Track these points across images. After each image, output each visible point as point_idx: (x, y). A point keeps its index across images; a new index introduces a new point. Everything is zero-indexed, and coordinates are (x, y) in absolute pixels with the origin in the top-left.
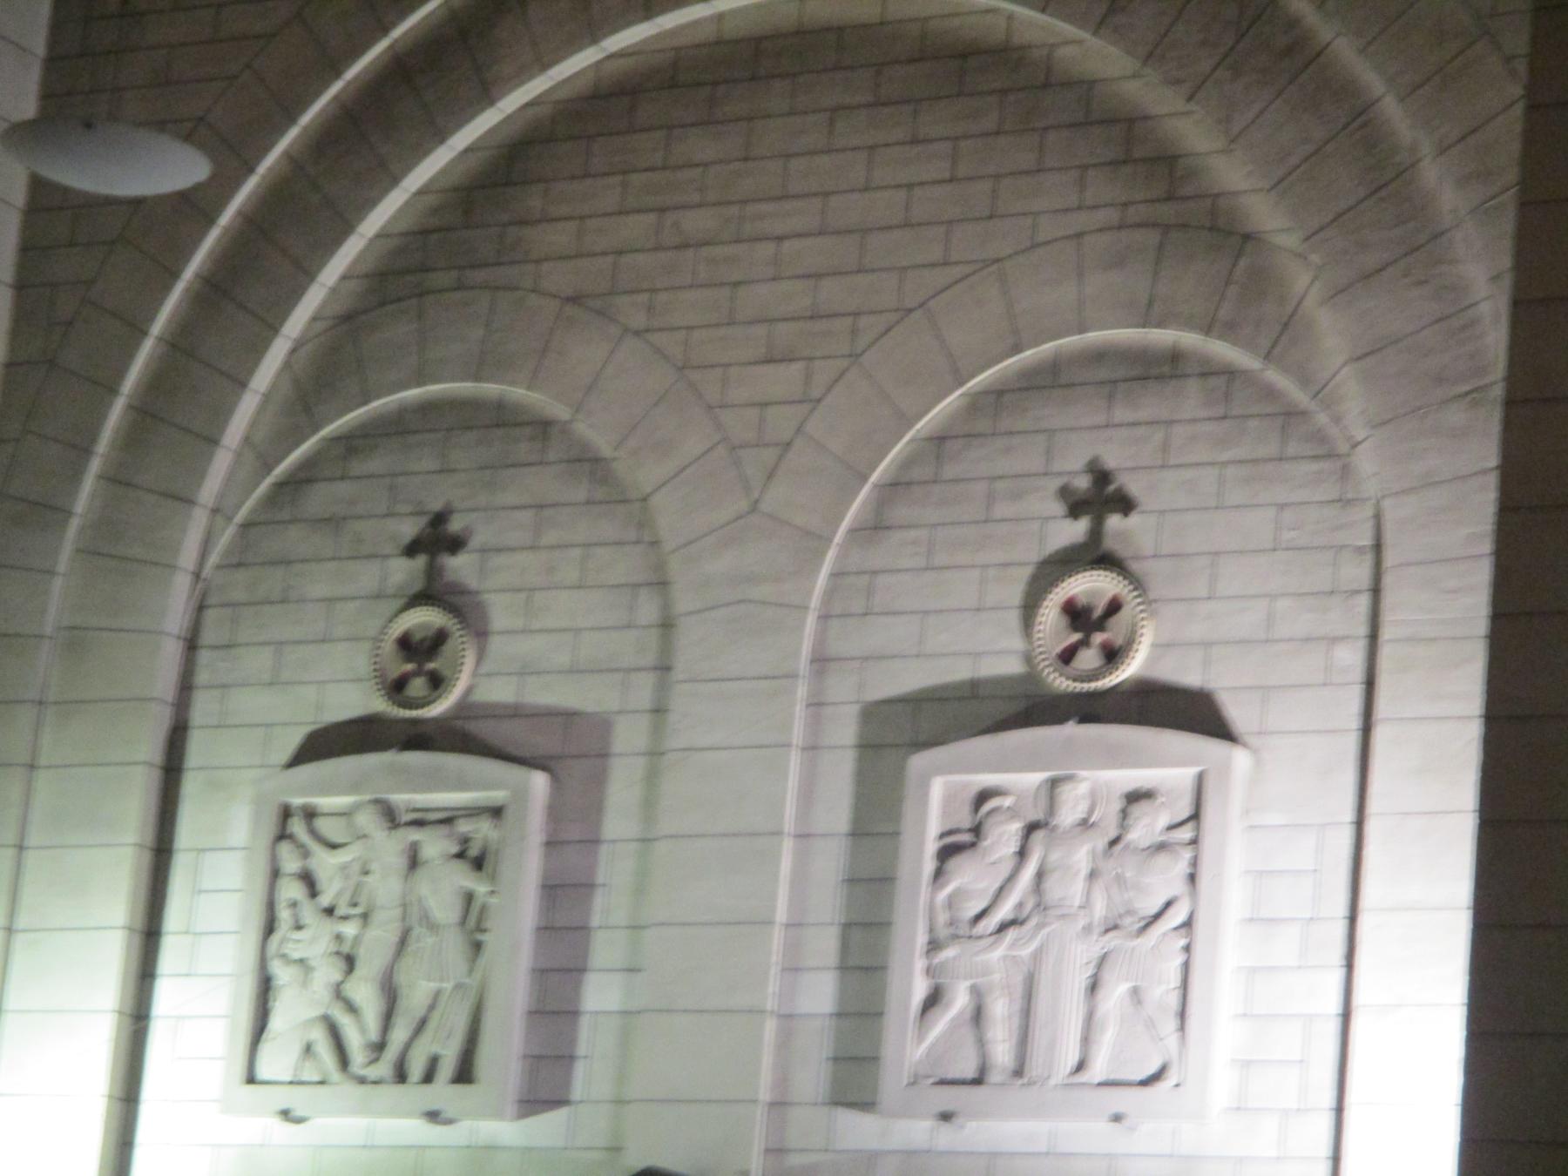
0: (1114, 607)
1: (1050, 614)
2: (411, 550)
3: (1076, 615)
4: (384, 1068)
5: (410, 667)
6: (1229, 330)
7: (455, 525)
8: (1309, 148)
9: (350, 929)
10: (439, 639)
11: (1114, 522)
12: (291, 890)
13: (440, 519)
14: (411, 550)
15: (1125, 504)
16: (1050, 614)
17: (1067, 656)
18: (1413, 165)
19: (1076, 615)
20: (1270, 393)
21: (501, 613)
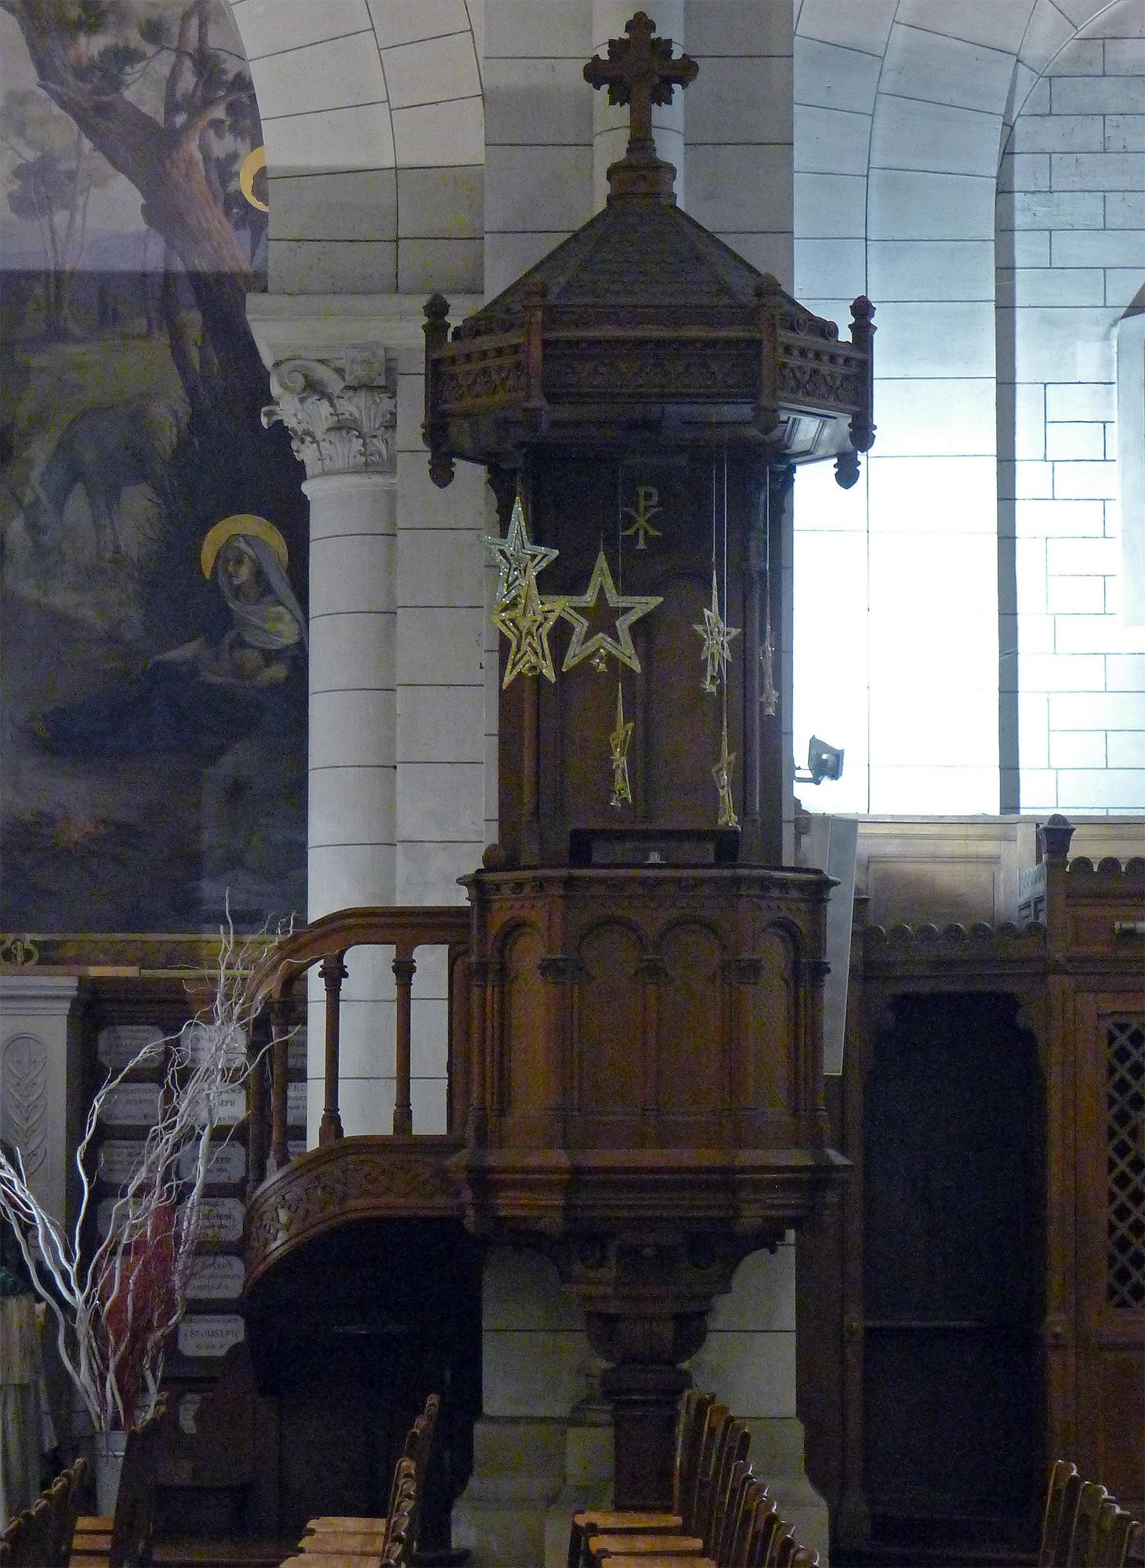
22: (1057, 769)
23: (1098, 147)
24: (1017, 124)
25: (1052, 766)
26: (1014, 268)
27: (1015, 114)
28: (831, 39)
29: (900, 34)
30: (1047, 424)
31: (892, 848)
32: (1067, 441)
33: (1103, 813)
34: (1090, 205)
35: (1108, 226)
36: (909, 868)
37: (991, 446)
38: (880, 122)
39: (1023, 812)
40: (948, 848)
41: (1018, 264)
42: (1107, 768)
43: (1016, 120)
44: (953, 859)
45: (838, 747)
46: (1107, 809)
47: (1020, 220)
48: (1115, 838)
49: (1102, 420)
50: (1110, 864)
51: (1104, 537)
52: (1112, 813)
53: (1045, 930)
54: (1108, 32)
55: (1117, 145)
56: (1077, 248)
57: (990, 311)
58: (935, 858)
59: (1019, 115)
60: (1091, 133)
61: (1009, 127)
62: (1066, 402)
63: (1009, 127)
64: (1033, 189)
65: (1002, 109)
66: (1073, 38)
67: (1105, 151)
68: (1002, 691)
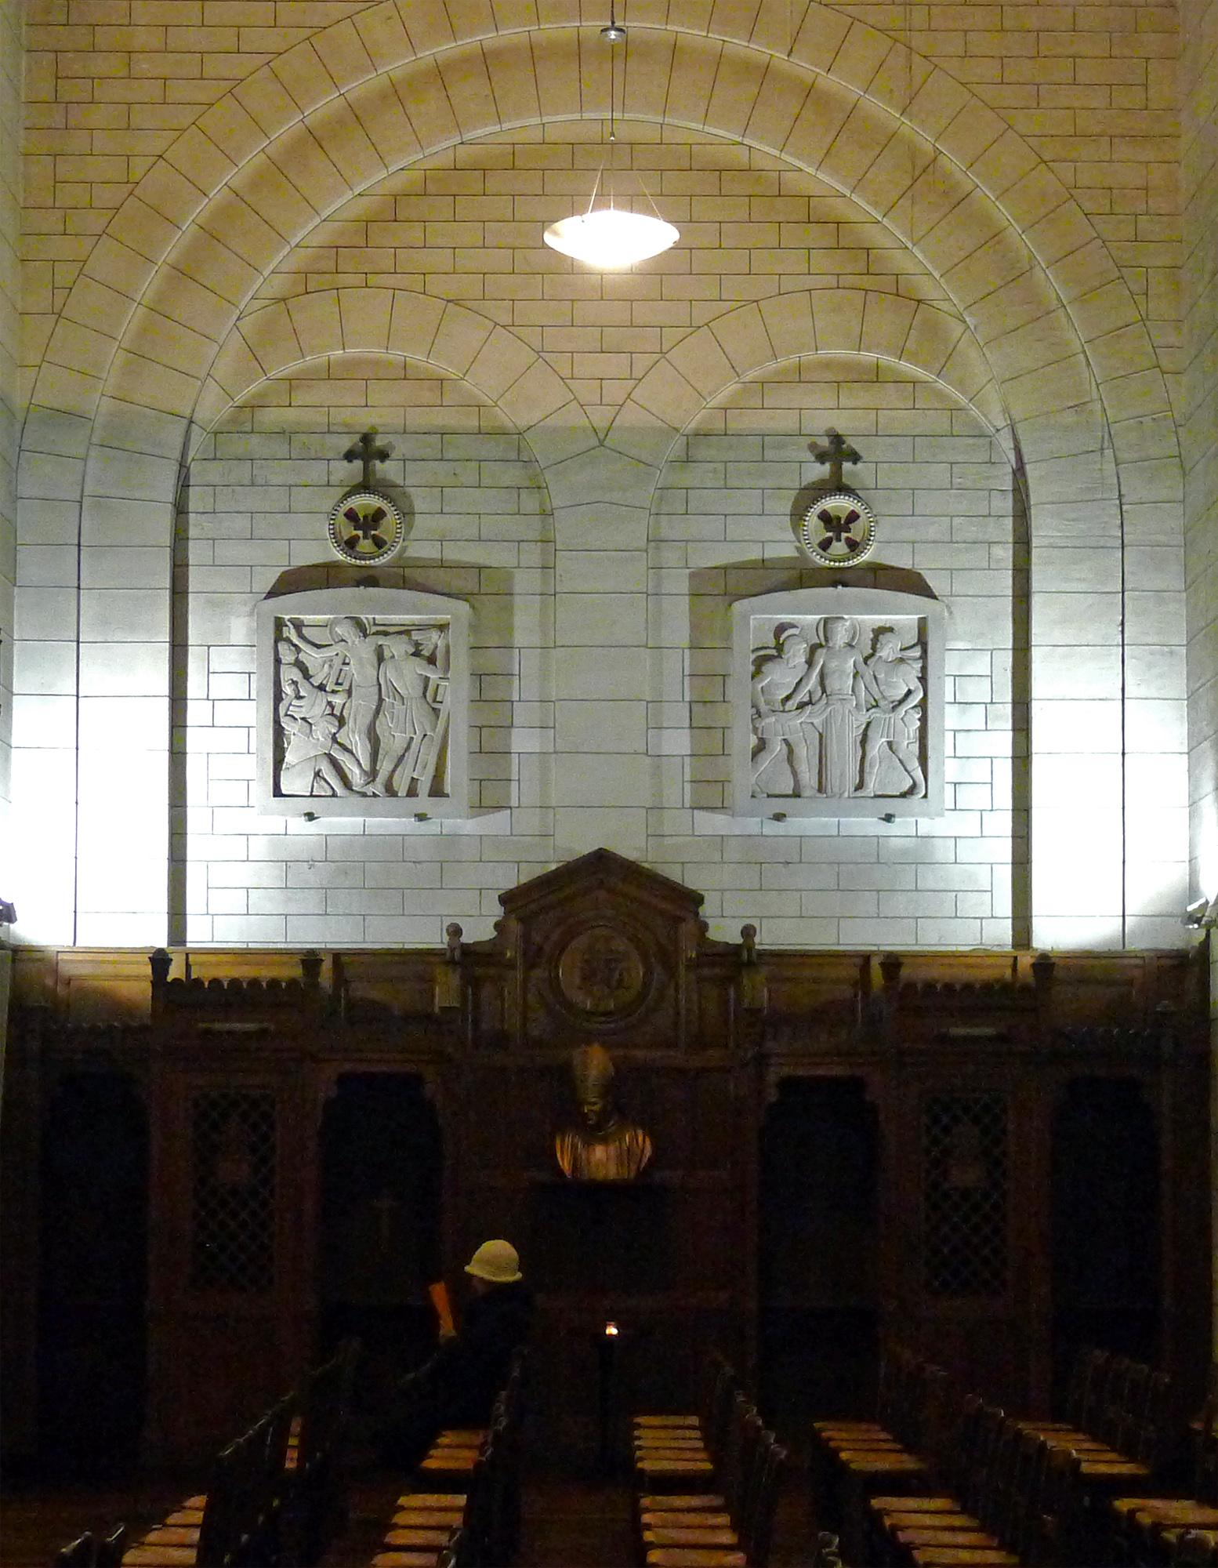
0: (853, 517)
1: (812, 519)
2: (350, 456)
3: (825, 517)
4: (378, 787)
5: (360, 533)
6: (914, 358)
7: (379, 442)
8: (963, 254)
9: (338, 700)
10: (379, 514)
11: (847, 466)
12: (289, 674)
13: (366, 439)
14: (350, 456)
15: (855, 457)
16: (812, 519)
17: (825, 545)
18: (1031, 268)
19: (825, 517)
20: (940, 395)
21: (421, 501)
22: (213, 915)
23: (246, 482)
24: (192, 466)
25: (209, 912)
26: (187, 566)
27: (189, 460)
28: (56, 406)
29: (107, 404)
30: (210, 675)
31: (85, 970)
32: (224, 686)
33: (401, 946)
34: (241, 523)
35: (723, 411)
36: (96, 983)
37: (165, 688)
38: (90, 464)
39: (189, 945)
40: (126, 970)
41: (190, 563)
42: (248, 914)
43: (190, 464)
44: (128, 978)
45: (9, 901)
46: (248, 942)
47: (193, 532)
48: (240, 964)
49: (247, 671)
50: (235, 982)
51: (249, 753)
52: (251, 946)
53: (34, 1020)
54: (255, 403)
55: (259, 480)
56: (231, 552)
57: (166, 595)
58: (116, 977)
59: (193, 460)
60: (243, 471)
61: (183, 465)
62: (221, 659)
63: (183, 465)
64: (201, 511)
65: (177, 454)
66: (231, 407)
67: (253, 485)
68: (184, 861)
